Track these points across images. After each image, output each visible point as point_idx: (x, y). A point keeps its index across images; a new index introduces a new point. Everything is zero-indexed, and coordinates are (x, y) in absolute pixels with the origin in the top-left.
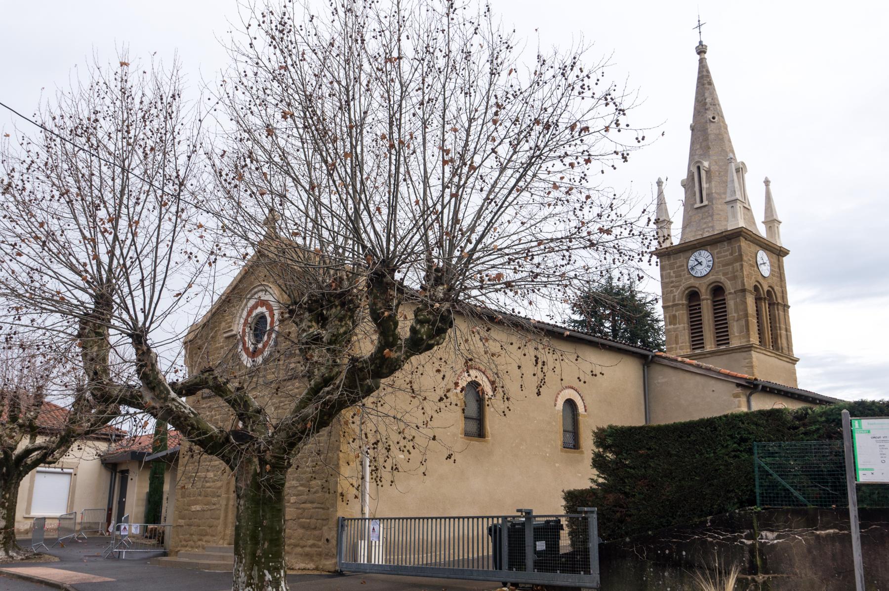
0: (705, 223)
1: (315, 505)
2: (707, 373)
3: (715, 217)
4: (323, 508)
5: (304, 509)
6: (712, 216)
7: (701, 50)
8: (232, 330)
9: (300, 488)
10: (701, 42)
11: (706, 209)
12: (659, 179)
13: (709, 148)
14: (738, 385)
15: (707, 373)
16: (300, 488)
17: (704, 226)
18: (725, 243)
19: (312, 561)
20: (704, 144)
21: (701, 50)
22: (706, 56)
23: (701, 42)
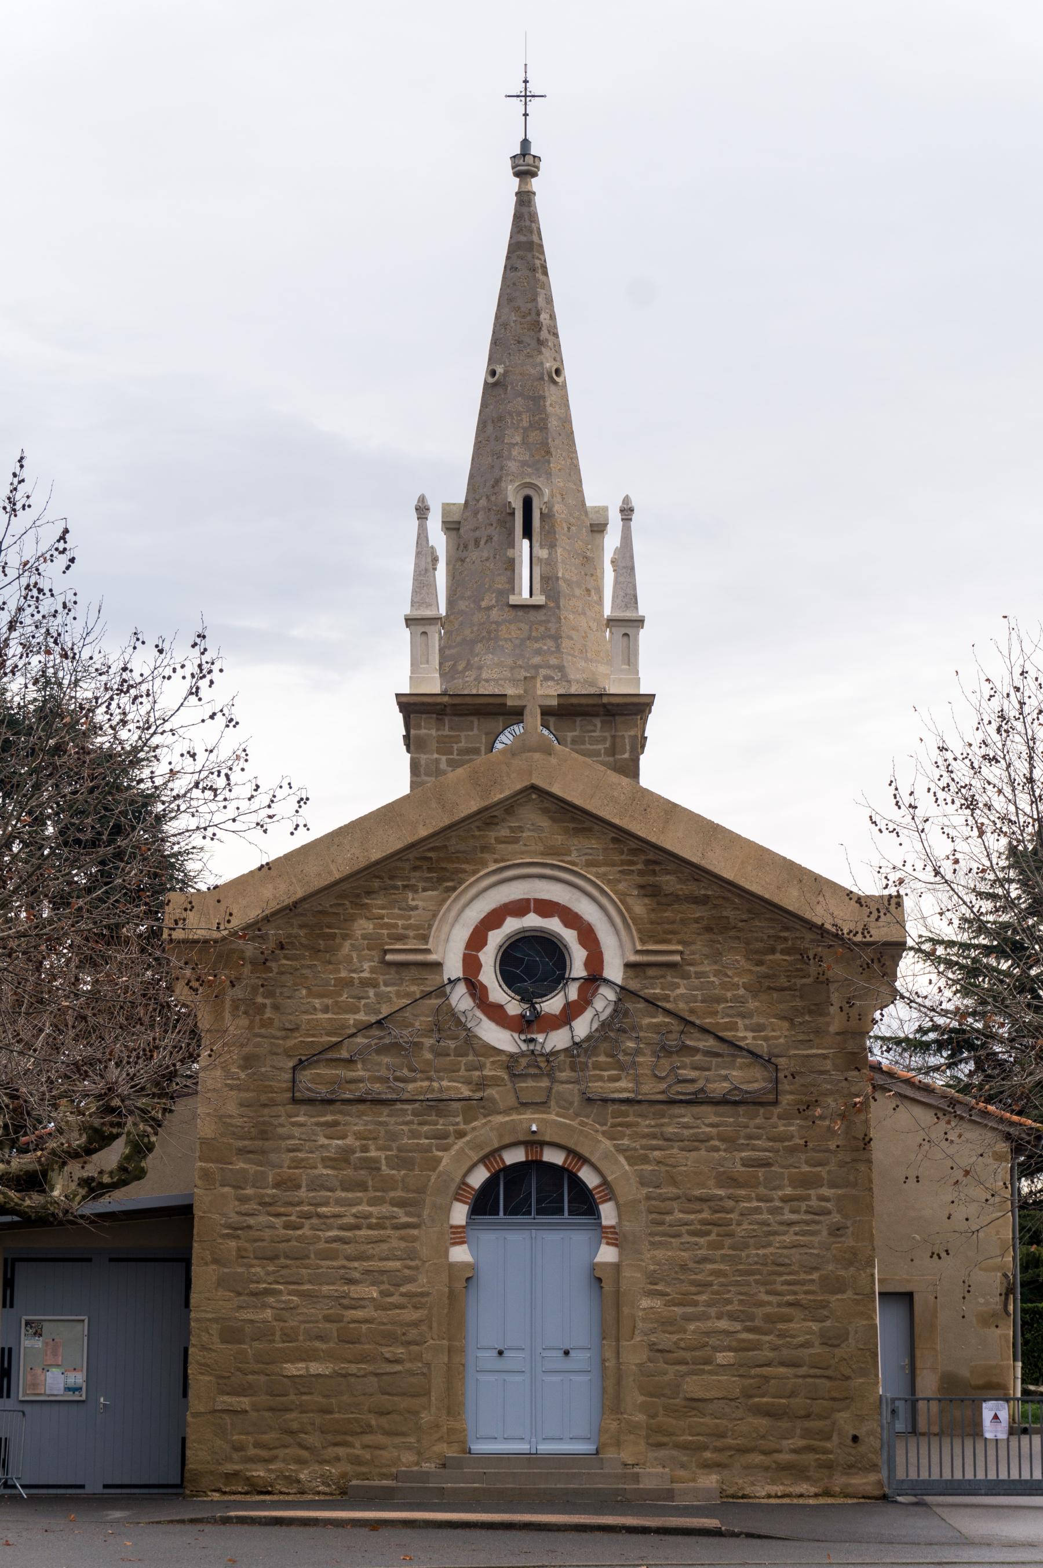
0: (538, 652)
1: (803, 1371)
2: (918, 1096)
3: (566, 644)
4: (828, 1378)
5: (766, 1378)
6: (557, 638)
7: (525, 165)
8: (428, 951)
9: (745, 1336)
10: (525, 143)
11: (540, 616)
12: (422, 499)
13: (548, 452)
14: (1008, 1137)
15: (918, 1096)
16: (745, 1336)
17: (537, 660)
18: (598, 722)
19: (807, 1479)
20: (534, 436)
21: (525, 165)
22: (535, 184)
23: (525, 143)
